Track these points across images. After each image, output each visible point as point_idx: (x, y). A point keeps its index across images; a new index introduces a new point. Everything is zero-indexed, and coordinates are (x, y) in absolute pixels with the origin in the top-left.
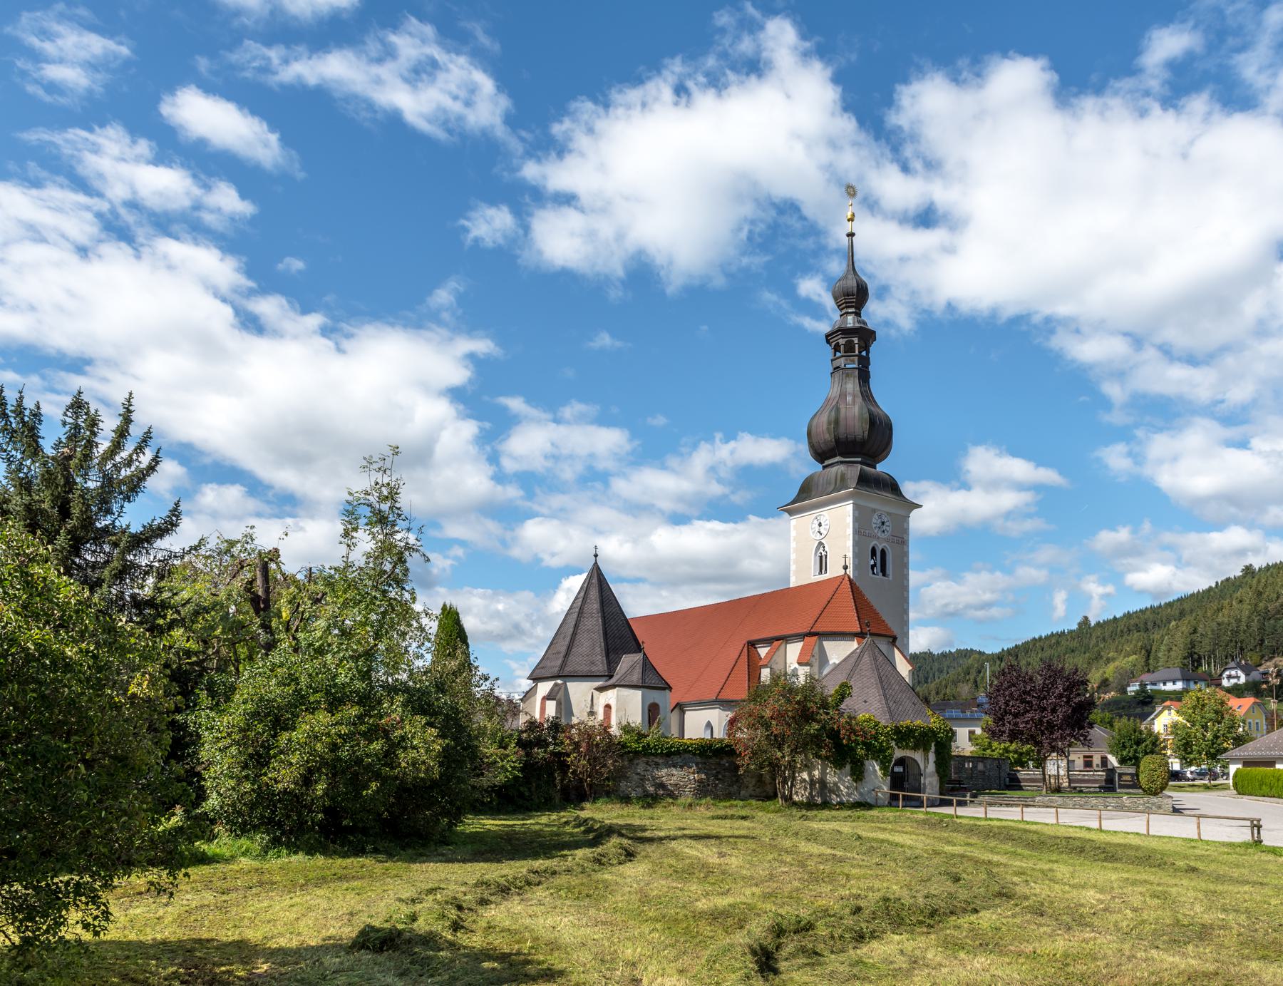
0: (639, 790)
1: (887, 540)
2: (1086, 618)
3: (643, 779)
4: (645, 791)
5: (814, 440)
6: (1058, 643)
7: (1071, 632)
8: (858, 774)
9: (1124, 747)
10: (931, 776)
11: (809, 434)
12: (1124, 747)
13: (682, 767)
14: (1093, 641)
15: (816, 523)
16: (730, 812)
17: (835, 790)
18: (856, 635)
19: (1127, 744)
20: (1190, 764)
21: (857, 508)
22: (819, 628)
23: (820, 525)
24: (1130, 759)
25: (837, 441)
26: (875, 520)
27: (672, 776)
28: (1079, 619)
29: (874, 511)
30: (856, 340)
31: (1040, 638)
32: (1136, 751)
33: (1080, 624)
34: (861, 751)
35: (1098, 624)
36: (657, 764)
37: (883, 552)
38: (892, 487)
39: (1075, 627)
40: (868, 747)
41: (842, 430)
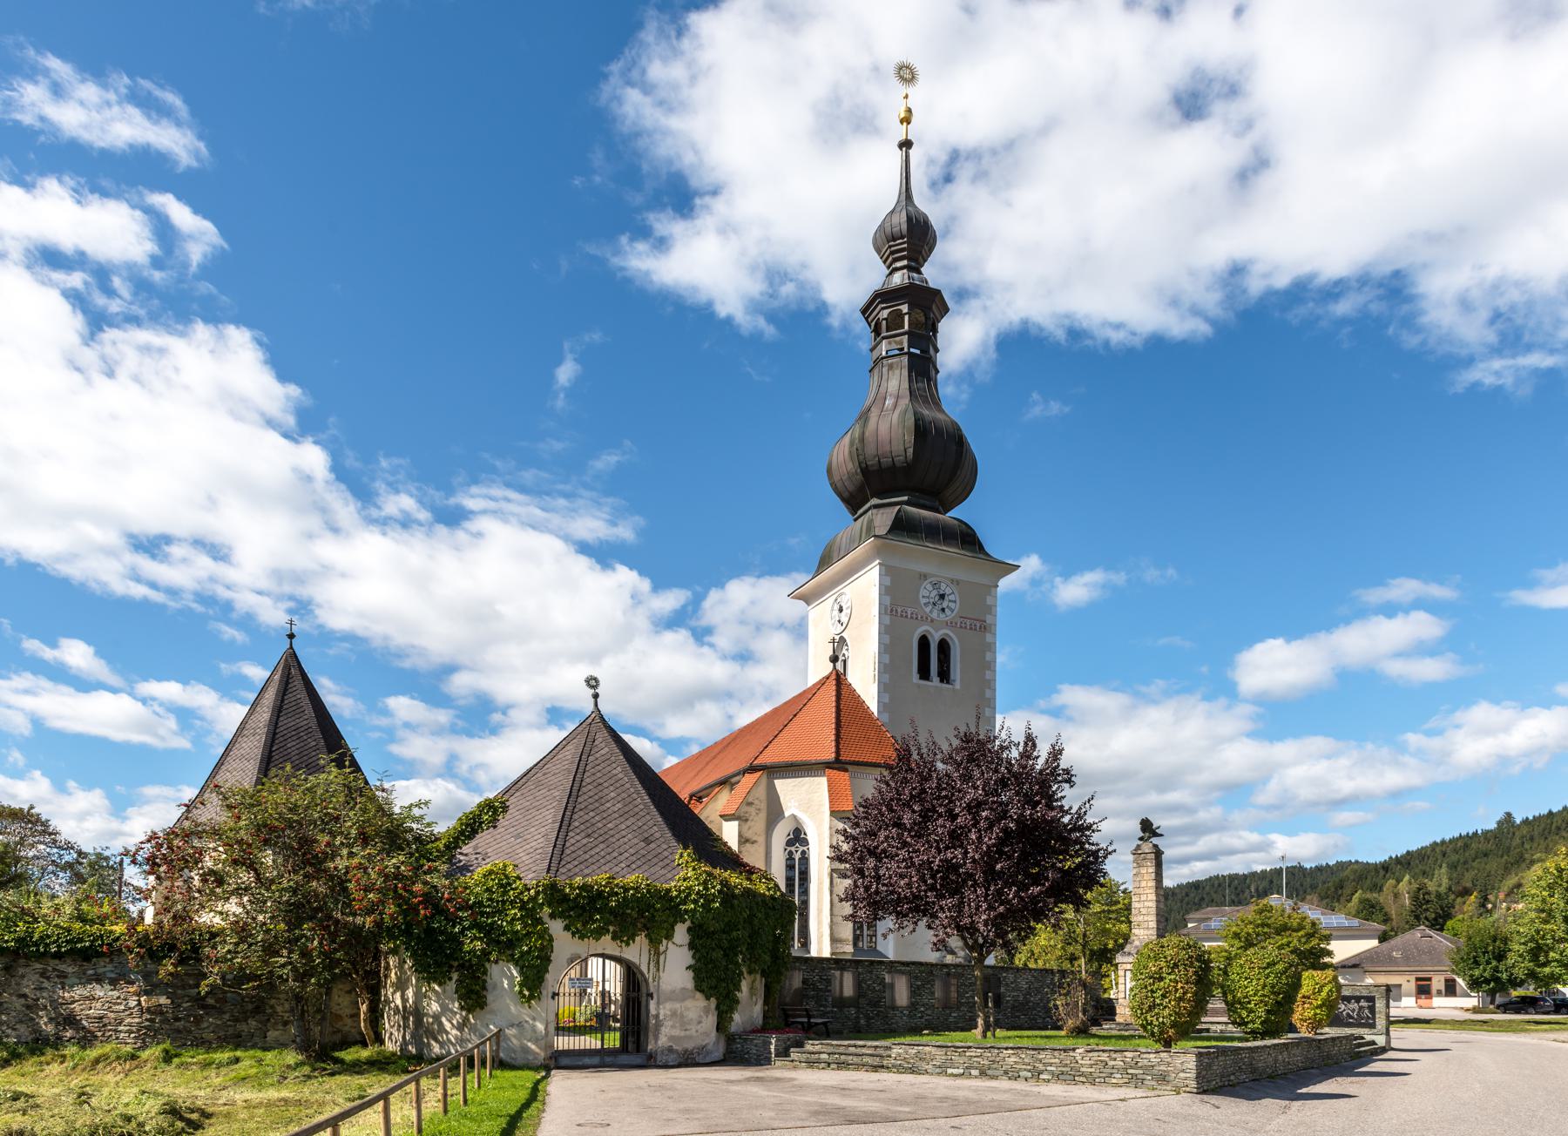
0: (22, 1029)
1: (948, 624)
2: (1509, 815)
3: (32, 1007)
4: (37, 1030)
5: (836, 478)
6: (1466, 846)
7: (1485, 833)
8: (474, 997)
9: (1477, 963)
10: (681, 996)
11: (829, 471)
12: (1477, 963)
13: (114, 983)
14: (1517, 841)
15: (837, 607)
16: (1025, 1043)
17: (435, 1032)
18: (828, 765)
19: (1482, 960)
20: (204, 881)
21: (886, 571)
22: (768, 758)
23: (841, 610)
24: (1487, 982)
25: (865, 470)
26: (926, 592)
27: (94, 1000)
28: (1499, 816)
29: (924, 577)
30: (905, 308)
31: (1443, 842)
32: (1496, 970)
33: (1499, 823)
34: (474, 944)
35: (1526, 822)
36: (63, 976)
37: (944, 646)
38: (967, 539)
39: (1492, 826)
40: (491, 934)
41: (870, 450)
